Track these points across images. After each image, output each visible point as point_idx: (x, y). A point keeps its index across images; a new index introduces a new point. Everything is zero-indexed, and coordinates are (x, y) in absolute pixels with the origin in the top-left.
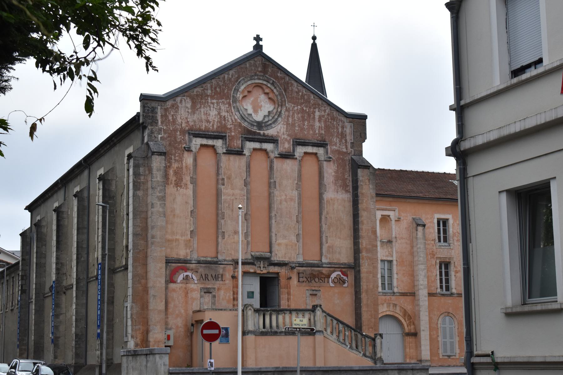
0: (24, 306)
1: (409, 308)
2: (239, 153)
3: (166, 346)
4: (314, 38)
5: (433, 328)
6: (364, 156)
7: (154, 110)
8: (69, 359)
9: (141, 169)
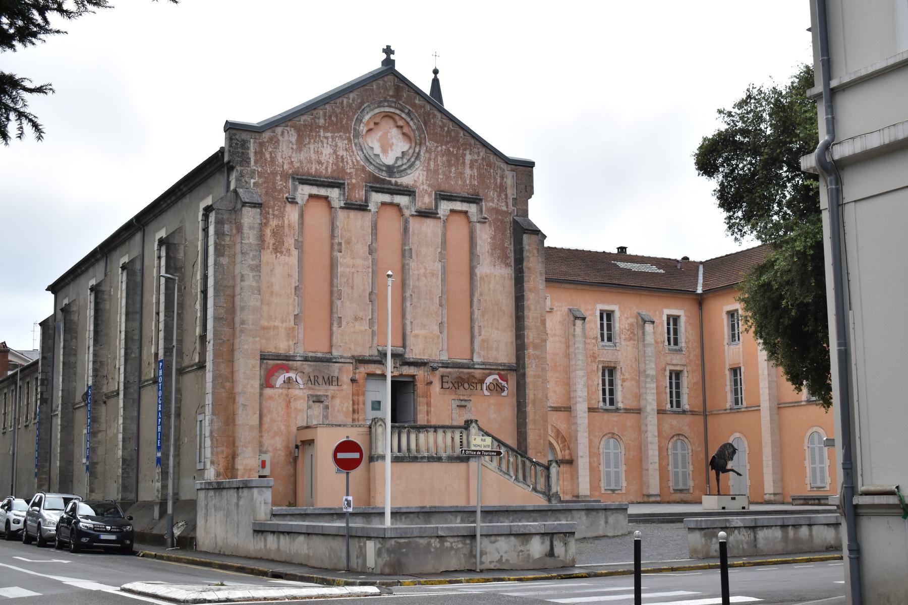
0: (45, 422)
1: (562, 427)
2: (363, 208)
3: (260, 477)
4: (436, 72)
5: (594, 454)
6: (530, 217)
7: (244, 144)
8: (113, 493)
9: (227, 227)
